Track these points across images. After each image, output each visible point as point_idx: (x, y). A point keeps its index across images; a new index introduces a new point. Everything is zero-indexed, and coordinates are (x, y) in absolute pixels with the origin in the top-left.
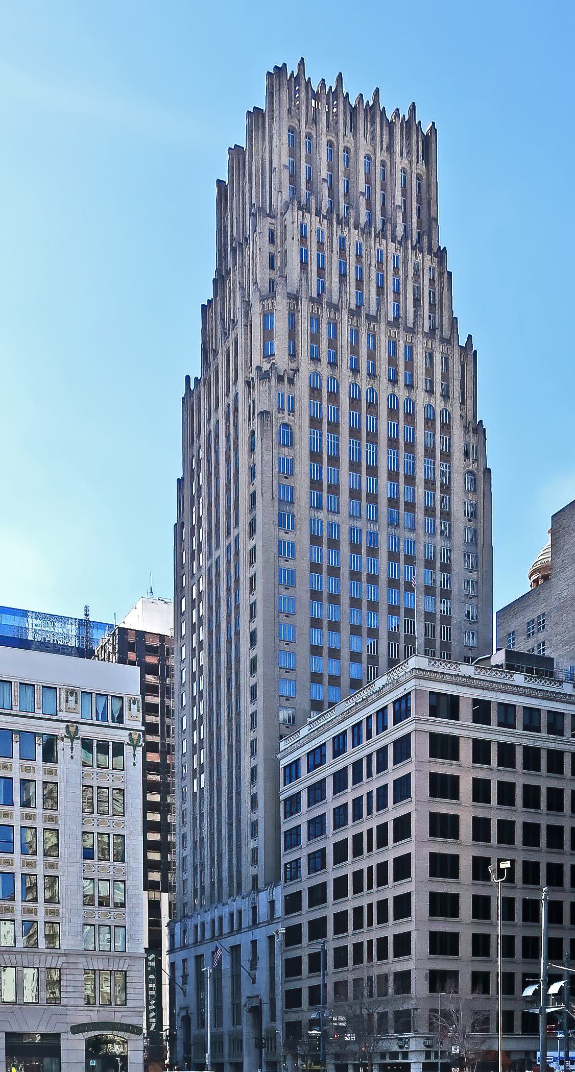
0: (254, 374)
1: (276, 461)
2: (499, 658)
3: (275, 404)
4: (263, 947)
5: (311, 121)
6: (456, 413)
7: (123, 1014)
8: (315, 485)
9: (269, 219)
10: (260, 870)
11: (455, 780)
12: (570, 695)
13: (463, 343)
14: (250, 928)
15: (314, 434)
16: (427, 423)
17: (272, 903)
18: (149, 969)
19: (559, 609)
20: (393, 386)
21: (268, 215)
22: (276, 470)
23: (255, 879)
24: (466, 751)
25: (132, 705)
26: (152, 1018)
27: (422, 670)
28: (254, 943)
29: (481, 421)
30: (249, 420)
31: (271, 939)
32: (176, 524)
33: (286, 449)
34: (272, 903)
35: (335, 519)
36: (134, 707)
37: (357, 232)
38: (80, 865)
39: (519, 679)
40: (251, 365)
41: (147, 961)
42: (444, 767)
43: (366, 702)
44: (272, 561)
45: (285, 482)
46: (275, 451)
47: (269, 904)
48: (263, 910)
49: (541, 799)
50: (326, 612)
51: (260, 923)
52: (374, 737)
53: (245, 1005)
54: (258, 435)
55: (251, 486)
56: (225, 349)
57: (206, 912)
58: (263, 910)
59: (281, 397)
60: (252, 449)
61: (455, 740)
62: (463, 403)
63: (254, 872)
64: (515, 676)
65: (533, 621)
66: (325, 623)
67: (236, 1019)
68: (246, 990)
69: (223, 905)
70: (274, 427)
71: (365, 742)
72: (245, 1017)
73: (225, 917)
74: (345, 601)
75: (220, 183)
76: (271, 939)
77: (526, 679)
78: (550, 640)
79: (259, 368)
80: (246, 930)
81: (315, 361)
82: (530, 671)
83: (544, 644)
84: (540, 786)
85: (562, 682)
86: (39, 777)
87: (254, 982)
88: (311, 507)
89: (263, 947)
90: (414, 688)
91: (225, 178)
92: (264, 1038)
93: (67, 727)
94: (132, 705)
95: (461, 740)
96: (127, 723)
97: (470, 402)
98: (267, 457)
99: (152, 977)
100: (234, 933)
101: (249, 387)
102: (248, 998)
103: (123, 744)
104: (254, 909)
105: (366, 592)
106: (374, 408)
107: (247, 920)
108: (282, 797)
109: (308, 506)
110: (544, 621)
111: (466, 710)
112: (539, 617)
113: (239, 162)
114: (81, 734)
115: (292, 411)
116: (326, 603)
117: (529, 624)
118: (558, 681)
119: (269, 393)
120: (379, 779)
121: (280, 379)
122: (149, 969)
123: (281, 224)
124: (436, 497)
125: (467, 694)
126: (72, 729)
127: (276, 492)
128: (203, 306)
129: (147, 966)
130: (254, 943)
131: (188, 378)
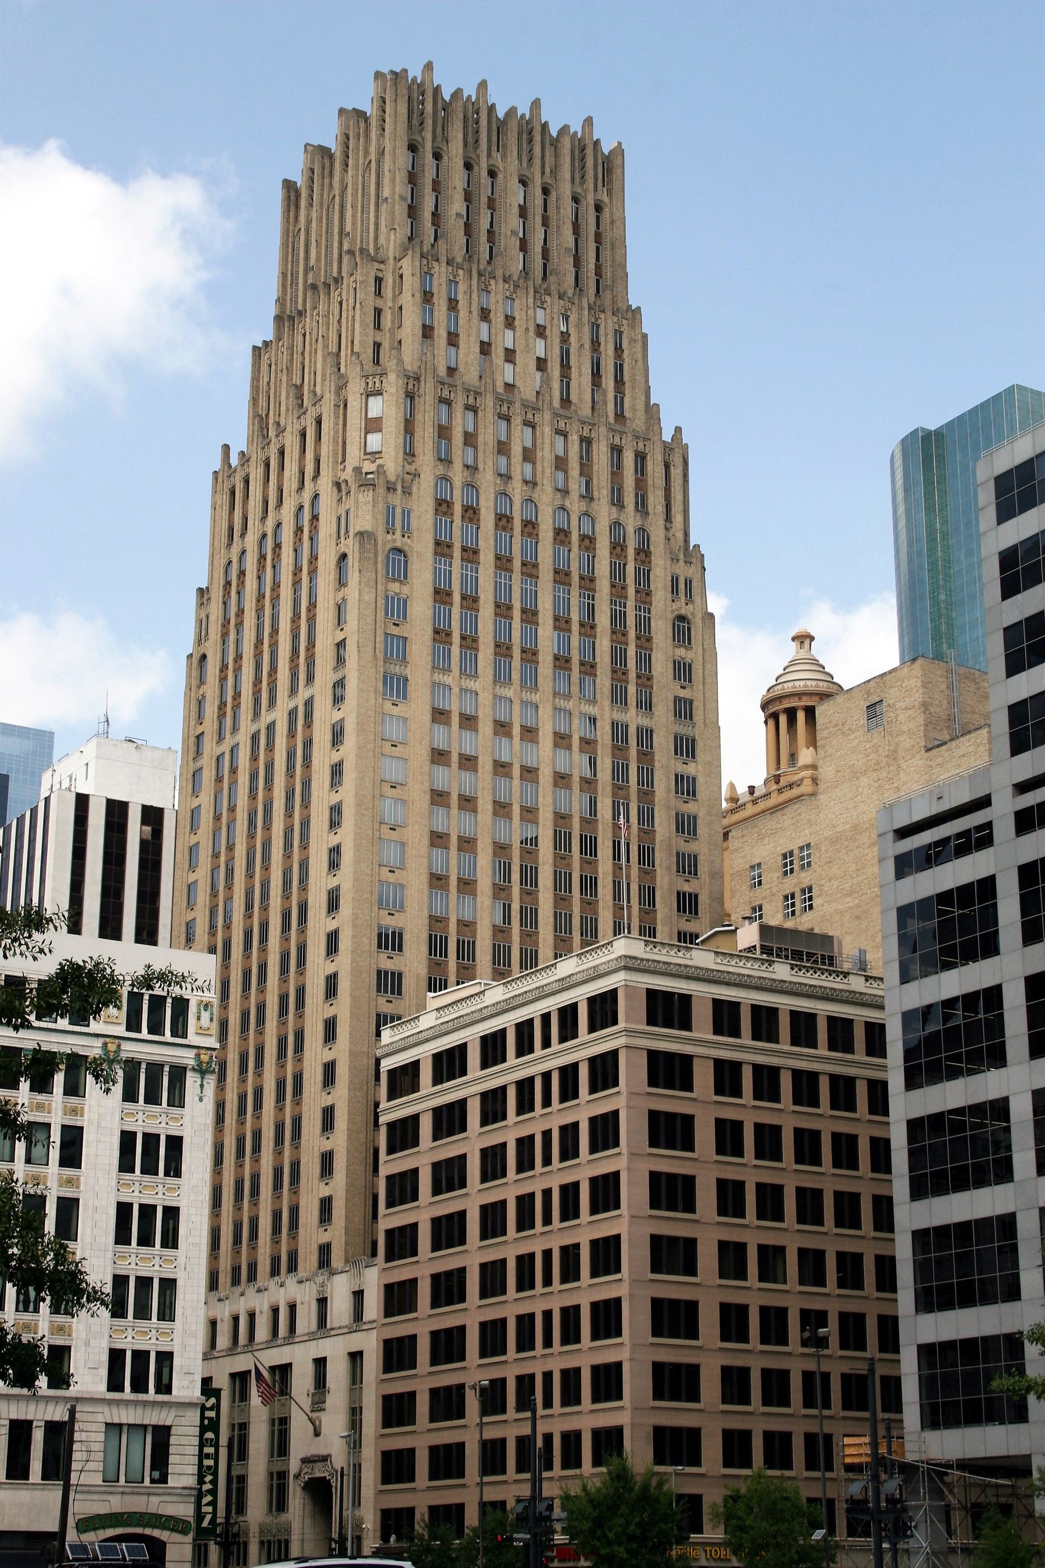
0: (348, 475)
1: (381, 602)
2: (748, 936)
3: (382, 519)
4: (337, 1373)
5: (440, 139)
6: (657, 534)
7: (162, 1498)
8: (441, 635)
9: (376, 265)
10: (336, 1234)
11: (688, 1121)
12: (861, 993)
13: (667, 437)
14: (312, 1337)
15: (440, 564)
16: (614, 548)
17: (358, 1295)
18: (206, 1422)
19: (833, 841)
20: (563, 498)
21: (374, 259)
22: (381, 614)
23: (325, 1250)
24: (703, 1077)
25: (203, 1011)
26: (207, 1504)
27: (635, 958)
28: (320, 1363)
29: (697, 547)
30: (339, 537)
31: (356, 1357)
32: (191, 655)
33: (397, 584)
34: (358, 1295)
35: (470, 684)
36: (205, 1016)
37: (507, 286)
38: (110, 1255)
39: (782, 971)
40: (344, 461)
41: (203, 1409)
42: (671, 1102)
43: (542, 994)
44: (372, 746)
45: (395, 630)
46: (380, 587)
47: (351, 1295)
48: (340, 1309)
49: (916, 1397)
50: (454, 823)
51: (332, 1329)
52: (555, 1046)
53: (297, 1476)
54: (353, 562)
55: (338, 632)
56: (298, 427)
57: (220, 1300)
58: (340, 1309)
59: (390, 511)
60: (341, 583)
61: (687, 1060)
62: (668, 518)
63: (324, 1238)
64: (776, 966)
65: (791, 853)
66: (454, 840)
67: (278, 1501)
68: (301, 1443)
69: (259, 1291)
70: (380, 553)
71: (538, 1052)
72: (296, 1499)
73: (261, 1312)
74: (485, 806)
75: (289, 186)
76: (356, 1357)
77: (792, 969)
78: (822, 885)
79: (357, 470)
80: (306, 1338)
81: (446, 464)
82: (797, 955)
83: (810, 889)
84: (820, 1132)
85: (849, 973)
86: (57, 1120)
87: (317, 1433)
88: (433, 667)
89: (337, 1373)
90: (623, 983)
91: (299, 180)
92: (334, 1540)
93: (105, 1044)
94: (203, 1011)
95: (695, 1061)
96: (192, 1038)
97: (678, 519)
98: (369, 597)
99: (210, 1435)
100: (280, 1342)
101: (340, 490)
102: (305, 1461)
103: (185, 1068)
104: (322, 1302)
105: (515, 789)
106: (534, 527)
107: (306, 1321)
108: (383, 1120)
109: (429, 667)
110: (809, 856)
111: (702, 1016)
112: (801, 848)
113: (323, 168)
114: (124, 1055)
115: (406, 532)
116: (454, 810)
117: (785, 857)
118: (842, 973)
119: (374, 506)
120: (563, 1113)
121: (390, 488)
122: (206, 1422)
123: (394, 271)
124: (628, 653)
125: (703, 993)
126: (112, 1047)
127: (380, 646)
128: (255, 348)
129: (203, 1417)
130: (320, 1363)
131: (226, 448)
